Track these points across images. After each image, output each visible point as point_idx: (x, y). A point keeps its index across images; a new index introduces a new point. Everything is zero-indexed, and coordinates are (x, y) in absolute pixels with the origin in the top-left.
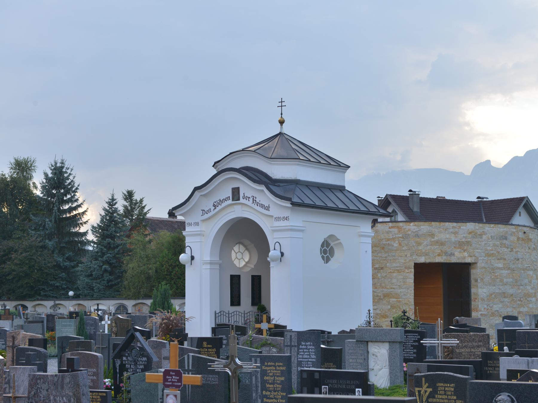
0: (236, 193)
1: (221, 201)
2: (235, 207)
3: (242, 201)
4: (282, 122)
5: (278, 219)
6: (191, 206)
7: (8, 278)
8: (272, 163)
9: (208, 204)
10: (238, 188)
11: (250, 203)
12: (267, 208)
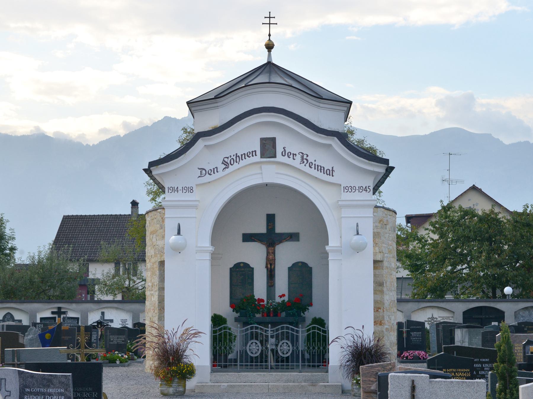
0: (268, 147)
1: (238, 158)
3: (279, 158)
5: (350, 189)
7: (432, 229)
8: (321, 105)
9: (214, 160)
10: (273, 140)
11: (297, 162)
12: (330, 172)
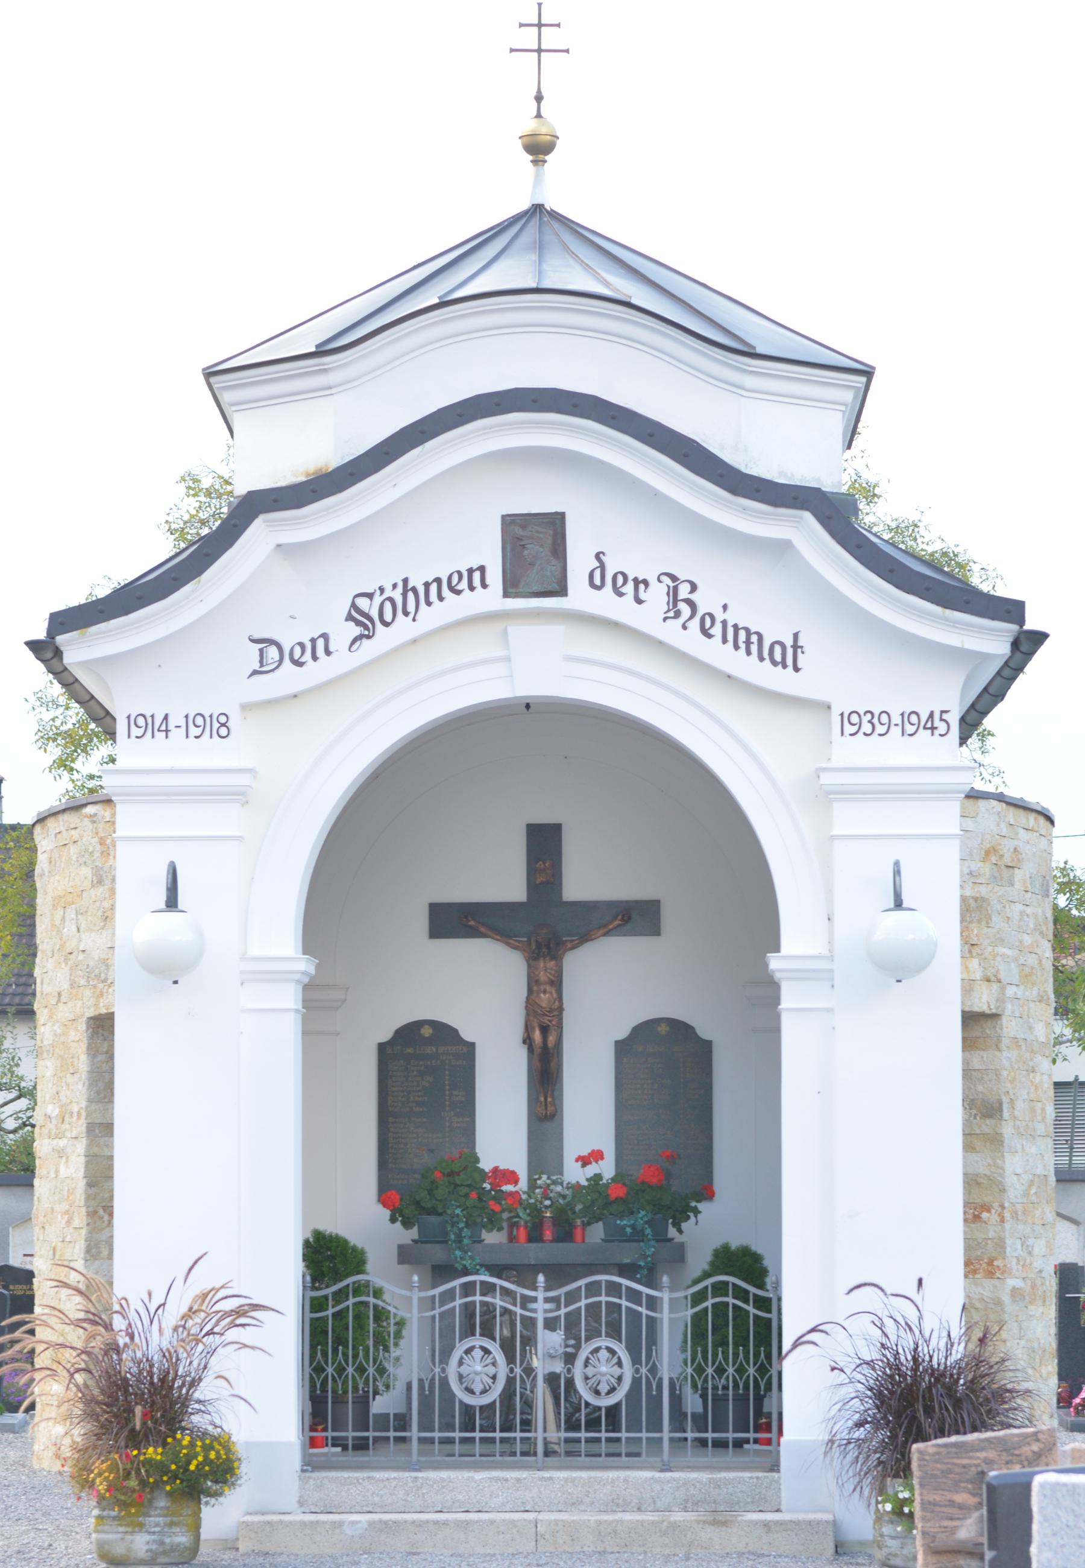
0: (534, 554)
1: (411, 596)
2: (517, 631)
3: (580, 595)
4: (539, 148)
5: (867, 722)
6: (196, 611)
8: (750, 381)
11: (650, 614)
12: (787, 655)
